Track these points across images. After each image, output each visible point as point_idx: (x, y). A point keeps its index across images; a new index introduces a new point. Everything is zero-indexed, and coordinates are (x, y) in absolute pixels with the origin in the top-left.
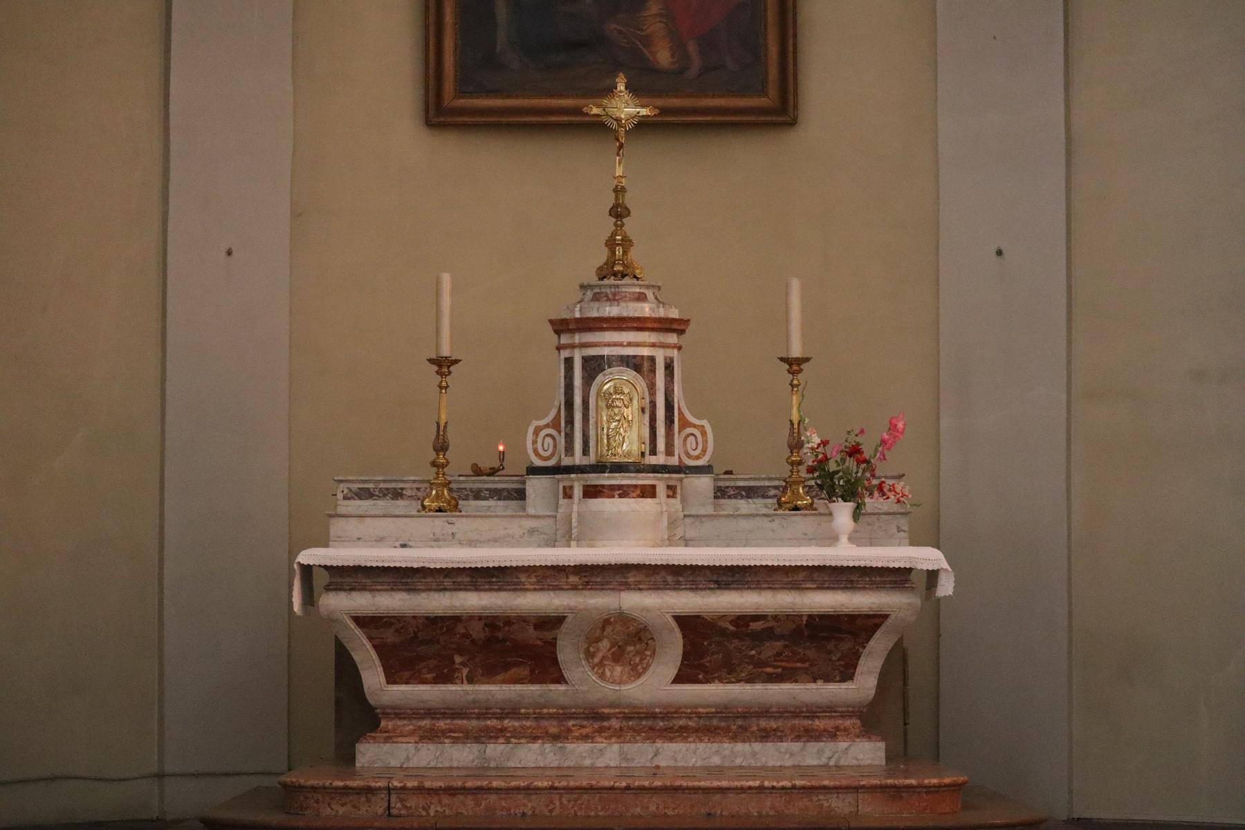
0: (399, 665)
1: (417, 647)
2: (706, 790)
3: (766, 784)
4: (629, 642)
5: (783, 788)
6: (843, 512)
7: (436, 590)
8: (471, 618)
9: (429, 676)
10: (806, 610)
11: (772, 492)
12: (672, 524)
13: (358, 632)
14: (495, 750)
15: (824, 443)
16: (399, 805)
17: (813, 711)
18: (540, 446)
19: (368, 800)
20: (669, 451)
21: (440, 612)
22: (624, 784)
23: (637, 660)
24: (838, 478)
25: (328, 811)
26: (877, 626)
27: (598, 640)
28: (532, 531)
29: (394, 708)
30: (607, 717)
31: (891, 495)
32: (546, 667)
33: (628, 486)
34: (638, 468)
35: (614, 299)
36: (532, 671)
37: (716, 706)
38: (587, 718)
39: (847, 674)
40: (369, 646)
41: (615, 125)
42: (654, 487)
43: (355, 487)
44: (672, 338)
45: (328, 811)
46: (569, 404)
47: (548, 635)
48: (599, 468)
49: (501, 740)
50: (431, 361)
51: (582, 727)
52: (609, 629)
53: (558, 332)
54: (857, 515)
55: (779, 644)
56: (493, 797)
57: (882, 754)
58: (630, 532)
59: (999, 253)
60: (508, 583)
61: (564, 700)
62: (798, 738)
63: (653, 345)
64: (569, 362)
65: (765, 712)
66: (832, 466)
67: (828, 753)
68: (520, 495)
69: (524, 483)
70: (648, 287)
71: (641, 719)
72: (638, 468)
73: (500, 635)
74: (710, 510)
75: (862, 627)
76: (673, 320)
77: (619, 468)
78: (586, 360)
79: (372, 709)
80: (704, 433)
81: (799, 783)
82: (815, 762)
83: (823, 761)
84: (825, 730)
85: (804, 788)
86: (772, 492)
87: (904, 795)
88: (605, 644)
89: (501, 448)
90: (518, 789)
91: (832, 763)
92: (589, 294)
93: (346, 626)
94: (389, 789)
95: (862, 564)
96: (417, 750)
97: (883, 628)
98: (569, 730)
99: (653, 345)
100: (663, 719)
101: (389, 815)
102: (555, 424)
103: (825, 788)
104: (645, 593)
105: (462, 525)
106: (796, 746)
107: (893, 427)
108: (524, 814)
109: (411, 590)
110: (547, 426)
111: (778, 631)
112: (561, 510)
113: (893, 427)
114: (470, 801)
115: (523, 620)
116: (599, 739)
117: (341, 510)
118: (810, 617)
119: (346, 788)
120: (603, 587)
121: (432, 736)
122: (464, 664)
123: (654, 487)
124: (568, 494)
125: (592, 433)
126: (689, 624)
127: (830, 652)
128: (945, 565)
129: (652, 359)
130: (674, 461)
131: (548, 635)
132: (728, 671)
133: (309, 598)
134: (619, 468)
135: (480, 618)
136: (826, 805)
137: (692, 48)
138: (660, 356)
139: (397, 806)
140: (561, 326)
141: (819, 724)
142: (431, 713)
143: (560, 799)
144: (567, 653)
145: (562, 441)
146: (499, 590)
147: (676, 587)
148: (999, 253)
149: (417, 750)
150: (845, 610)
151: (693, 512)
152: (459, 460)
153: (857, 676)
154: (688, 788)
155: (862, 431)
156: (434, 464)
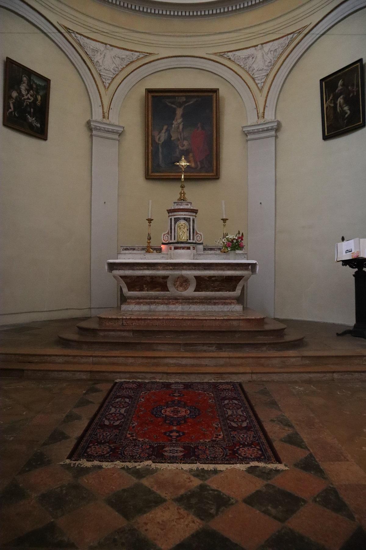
0: (131, 287)
1: (134, 283)
2: (202, 320)
4: (184, 282)
12: (194, 255)
13: (121, 279)
14: (153, 307)
18: (166, 239)
20: (193, 239)
21: (139, 275)
28: (163, 257)
30: (179, 299)
32: (165, 288)
44: (194, 214)
47: (165, 280)
48: (178, 243)
53: (169, 213)
56: (149, 321)
61: (170, 296)
62: (222, 304)
64: (171, 219)
65: (215, 298)
75: (238, 279)
77: (182, 243)
88: (178, 283)
90: (155, 319)
94: (123, 319)
102: (168, 233)
106: (222, 306)
114: (143, 322)
115: (159, 277)
120: (178, 269)
121: (139, 303)
124: (171, 249)
126: (197, 278)
129: (190, 218)
130: (194, 242)
131: (165, 280)
132: (207, 289)
134: (182, 243)
137: (199, 163)
138: (191, 218)
140: (170, 211)
142: (139, 298)
144: (169, 284)
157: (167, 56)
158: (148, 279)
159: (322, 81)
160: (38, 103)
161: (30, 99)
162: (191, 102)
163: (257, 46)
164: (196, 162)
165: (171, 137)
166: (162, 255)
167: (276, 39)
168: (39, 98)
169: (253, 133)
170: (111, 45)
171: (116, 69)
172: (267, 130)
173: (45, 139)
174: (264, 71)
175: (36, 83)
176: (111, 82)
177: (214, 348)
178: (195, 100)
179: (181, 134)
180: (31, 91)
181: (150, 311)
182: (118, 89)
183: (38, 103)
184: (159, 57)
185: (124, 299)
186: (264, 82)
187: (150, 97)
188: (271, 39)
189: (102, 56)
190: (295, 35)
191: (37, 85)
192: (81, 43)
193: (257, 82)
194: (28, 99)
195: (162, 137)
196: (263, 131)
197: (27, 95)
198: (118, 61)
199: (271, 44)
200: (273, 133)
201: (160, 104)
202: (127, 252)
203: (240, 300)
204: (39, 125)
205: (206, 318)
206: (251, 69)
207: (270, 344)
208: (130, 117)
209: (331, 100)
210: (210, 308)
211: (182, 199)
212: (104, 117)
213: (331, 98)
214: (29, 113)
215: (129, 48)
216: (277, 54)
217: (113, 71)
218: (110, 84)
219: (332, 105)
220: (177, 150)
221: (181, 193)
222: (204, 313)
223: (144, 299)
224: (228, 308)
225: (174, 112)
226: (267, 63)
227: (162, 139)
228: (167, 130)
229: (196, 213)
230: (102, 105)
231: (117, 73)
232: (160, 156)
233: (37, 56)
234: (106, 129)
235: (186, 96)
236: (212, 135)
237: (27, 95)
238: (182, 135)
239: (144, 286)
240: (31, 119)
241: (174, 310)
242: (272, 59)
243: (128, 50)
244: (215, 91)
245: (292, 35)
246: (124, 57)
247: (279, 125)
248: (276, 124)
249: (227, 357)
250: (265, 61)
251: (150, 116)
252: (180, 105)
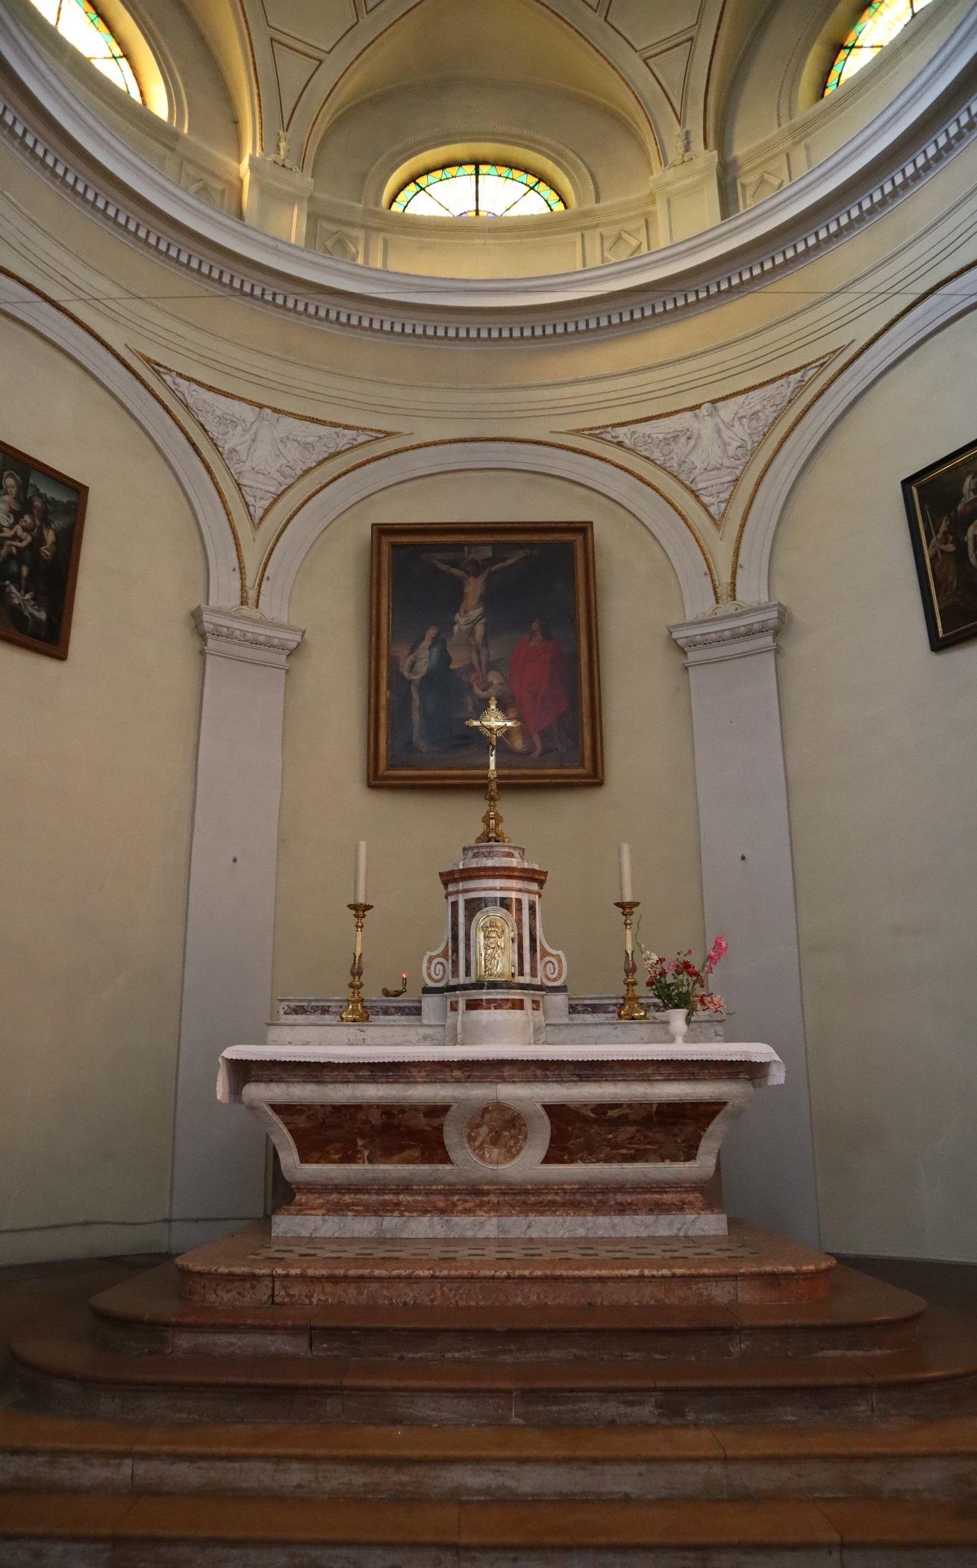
1: (325, 1131)
2: (586, 1280)
3: (646, 1272)
4: (504, 1127)
5: (663, 1277)
6: (677, 1018)
7: (342, 1082)
8: (370, 1106)
9: (336, 1157)
10: (656, 1099)
11: (612, 1008)
12: (537, 1030)
13: (275, 1118)
14: (391, 1223)
15: (661, 960)
16: (283, 1293)
17: (662, 1187)
18: (433, 972)
19: (253, 1287)
20: (534, 974)
21: (343, 1101)
22: (505, 1273)
23: (512, 1143)
24: (675, 990)
25: (213, 1298)
26: (717, 1112)
27: (478, 1126)
28: (425, 1038)
29: (308, 1183)
30: (487, 1193)
31: (711, 1006)
32: (434, 1149)
33: (502, 1000)
34: (509, 986)
35: (490, 855)
36: (423, 1153)
37: (578, 1183)
38: (469, 1194)
39: (690, 1156)
40: (285, 1131)
41: (489, 734)
42: (522, 1001)
43: (293, 1004)
44: (535, 887)
45: (213, 1298)
46: (455, 938)
47: (436, 1122)
48: (479, 985)
49: (396, 1213)
50: (351, 907)
51: (466, 1201)
52: (487, 1117)
53: (446, 884)
54: (688, 1021)
55: (632, 1129)
56: (375, 1286)
57: (724, 1225)
58: (504, 1035)
59: (743, 858)
60: (401, 1077)
61: (452, 1179)
62: (651, 1211)
63: (520, 890)
64: (455, 905)
65: (621, 1188)
66: (669, 979)
67: (677, 1225)
68: (417, 1011)
69: (420, 1002)
70: (515, 848)
71: (515, 1194)
72: (509, 986)
73: (396, 1121)
74: (566, 1021)
75: (703, 1113)
76: (534, 871)
77: (494, 985)
78: (468, 902)
79: (287, 1184)
80: (560, 961)
81: (678, 1271)
82: (666, 1233)
83: (674, 1232)
84: (673, 1204)
85: (682, 1276)
86: (612, 1008)
87: (782, 1282)
88: (484, 1130)
90: (399, 1277)
91: (681, 1234)
92: (470, 854)
93: (265, 1112)
94: (273, 1277)
95: (704, 1058)
96: (324, 1221)
97: (722, 1114)
98: (454, 1205)
99: (520, 890)
100: (533, 1194)
101: (273, 1303)
102: (444, 954)
103: (704, 1276)
104: (518, 1085)
105: (371, 1032)
106: (649, 1219)
107: (718, 944)
108: (405, 1304)
109: (320, 1082)
110: (438, 956)
111: (631, 1118)
112: (449, 1021)
113: (718, 944)
114: (352, 1290)
115: (414, 1108)
116: (480, 1213)
117: (282, 1021)
118: (660, 1105)
119: (231, 1274)
120: (482, 1080)
121: (337, 1209)
122: (365, 1146)
123: (522, 1001)
124: (454, 1008)
125: (473, 958)
126: (556, 1112)
127: (676, 1135)
128: (777, 1058)
129: (519, 901)
130: (537, 981)
131: (436, 1122)
132: (588, 1152)
133: (236, 1091)
134: (494, 985)
135: (378, 1107)
136: (705, 1293)
137: (536, 738)
138: (526, 899)
139: (281, 1295)
140: (449, 878)
141: (667, 1198)
142: (338, 1189)
143: (442, 1287)
144: (452, 1138)
145: (449, 967)
146: (395, 1082)
147: (545, 1080)
148: (743, 858)
149: (324, 1221)
150: (690, 1099)
151: (553, 1021)
152: (372, 993)
153: (699, 1156)
154: (568, 1278)
155: (690, 952)
156: (351, 986)
157: (437, 439)
158: (376, 1119)
159: (906, 483)
160: (46, 551)
161: (21, 541)
162: (509, 562)
163: (698, 407)
164: (524, 731)
165: (450, 662)
166: (422, 1031)
167: (754, 388)
168: (50, 536)
169: (707, 643)
170: (275, 410)
171: (288, 471)
172: (746, 634)
173: (61, 656)
174: (724, 472)
175: (41, 496)
176: (272, 505)
177: (647, 1411)
178: (521, 553)
179: (478, 652)
180: (27, 518)
181: (380, 1241)
182: (292, 522)
183: (46, 551)
184: (415, 442)
185: (283, 1193)
186: (728, 501)
187: (385, 548)
188: (741, 388)
189: (248, 437)
190: (811, 373)
191: (46, 501)
192: (190, 401)
193: (706, 500)
194: (15, 537)
195: (424, 659)
196: (736, 636)
197: (11, 527)
198: (293, 453)
199: (741, 399)
200: (768, 640)
201: (413, 571)
202: (300, 1018)
203: (710, 1194)
204: (42, 616)
205: (604, 1273)
206: (686, 467)
207: (884, 1387)
208: (325, 603)
209: (945, 533)
210: (603, 1225)
211: (490, 837)
212: (244, 602)
213: (943, 528)
214: (16, 579)
215: (328, 419)
216: (760, 425)
217: (277, 475)
218: (267, 511)
219: (950, 548)
220: (469, 700)
221: (486, 820)
222: (586, 1244)
223: (359, 1190)
224: (671, 1224)
225: (458, 587)
226: (731, 451)
227: (422, 668)
228: (435, 641)
229: (541, 883)
230: (242, 569)
231: (289, 481)
232: (416, 717)
233: (60, 429)
234: (249, 636)
235: (495, 545)
236: (576, 656)
237: (11, 527)
238: (483, 652)
239: (360, 1142)
240: (18, 597)
241: (470, 1234)
242: (746, 438)
243: (322, 423)
244: (583, 529)
245: (800, 374)
246: (311, 439)
247: (783, 613)
248: (775, 614)
249: (716, 1459)
250: (726, 444)
251: (385, 601)
252: (477, 568)
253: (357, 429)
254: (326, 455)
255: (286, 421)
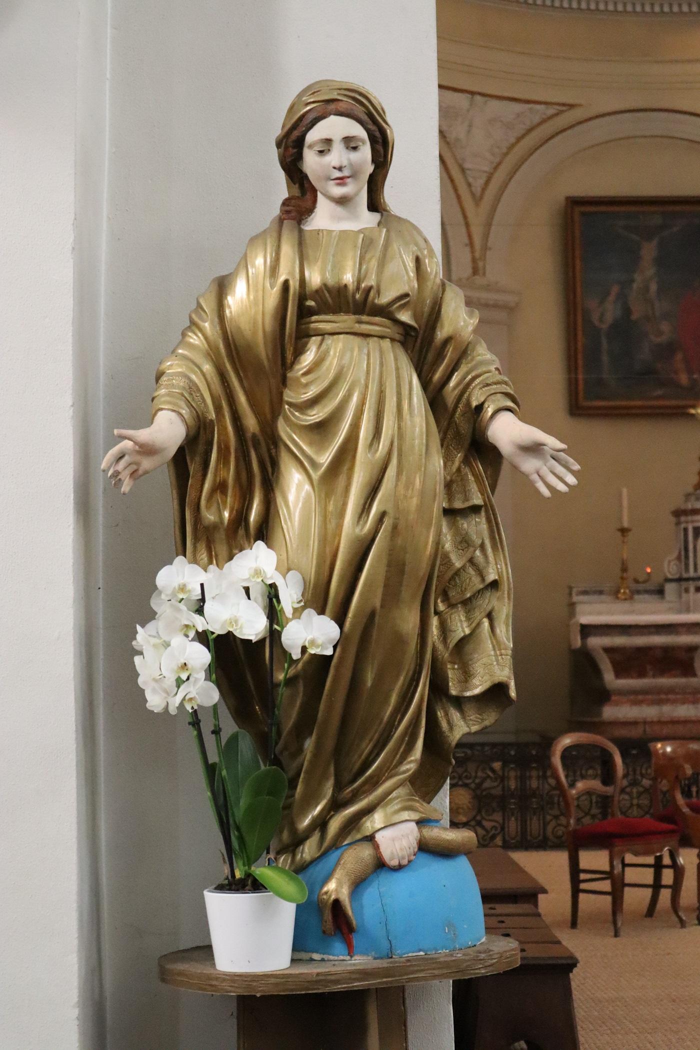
0: (621, 670)
1: (630, 662)
18: (671, 569)
32: (687, 669)
64: (686, 530)
89: (649, 570)
105: (638, 606)
124: (687, 591)
139: (648, 729)
140: (678, 513)
162: (675, 229)
187: (577, 217)
227: (609, 318)
232: (605, 358)
253: (546, 103)
254: (523, 132)
255: (494, 104)
